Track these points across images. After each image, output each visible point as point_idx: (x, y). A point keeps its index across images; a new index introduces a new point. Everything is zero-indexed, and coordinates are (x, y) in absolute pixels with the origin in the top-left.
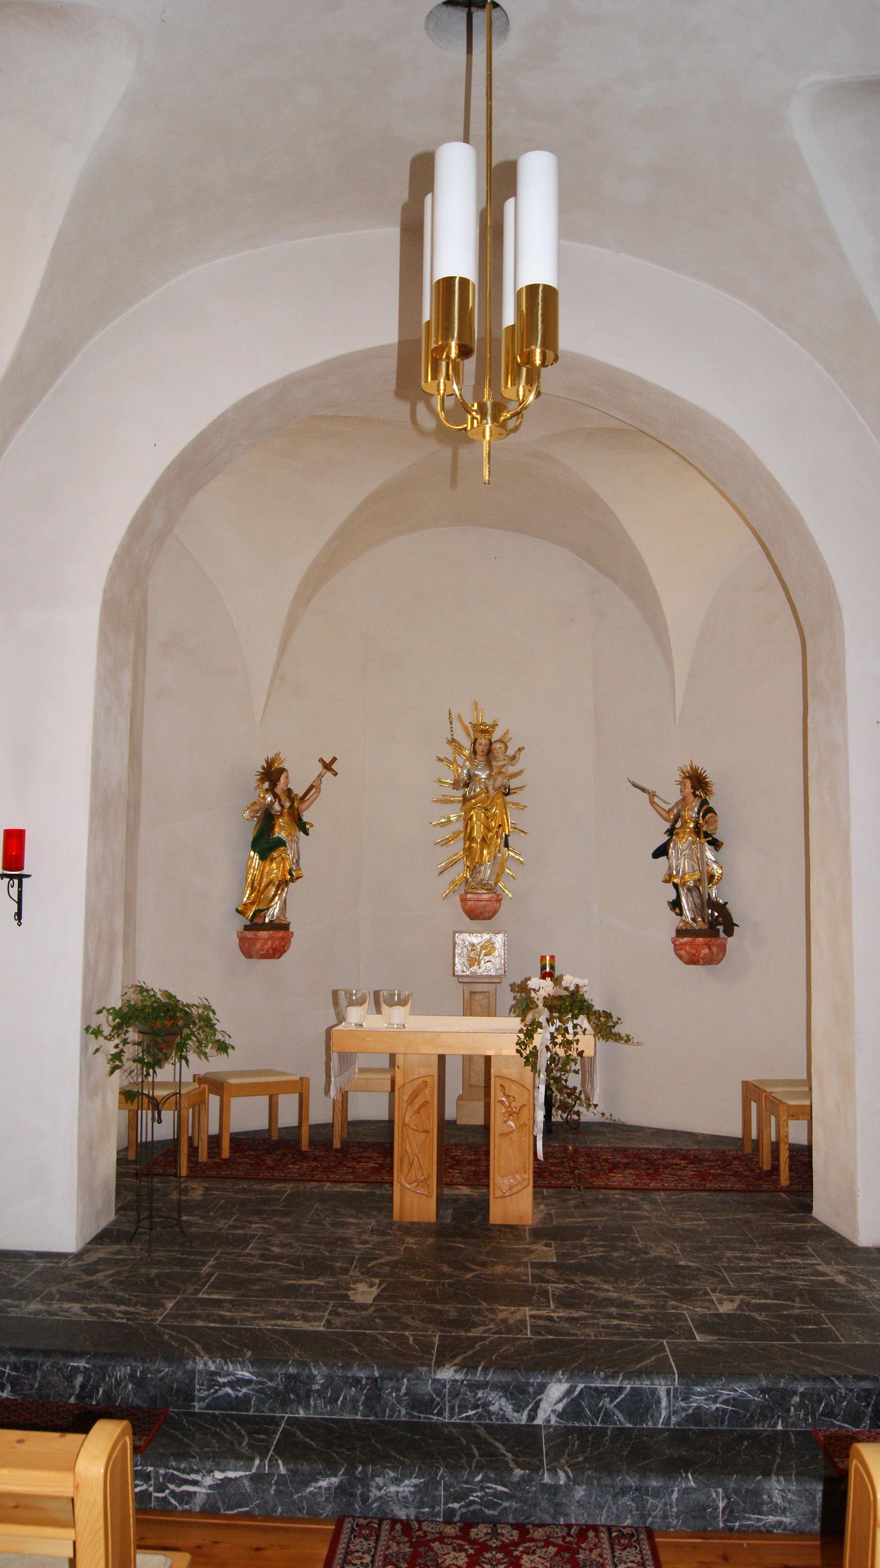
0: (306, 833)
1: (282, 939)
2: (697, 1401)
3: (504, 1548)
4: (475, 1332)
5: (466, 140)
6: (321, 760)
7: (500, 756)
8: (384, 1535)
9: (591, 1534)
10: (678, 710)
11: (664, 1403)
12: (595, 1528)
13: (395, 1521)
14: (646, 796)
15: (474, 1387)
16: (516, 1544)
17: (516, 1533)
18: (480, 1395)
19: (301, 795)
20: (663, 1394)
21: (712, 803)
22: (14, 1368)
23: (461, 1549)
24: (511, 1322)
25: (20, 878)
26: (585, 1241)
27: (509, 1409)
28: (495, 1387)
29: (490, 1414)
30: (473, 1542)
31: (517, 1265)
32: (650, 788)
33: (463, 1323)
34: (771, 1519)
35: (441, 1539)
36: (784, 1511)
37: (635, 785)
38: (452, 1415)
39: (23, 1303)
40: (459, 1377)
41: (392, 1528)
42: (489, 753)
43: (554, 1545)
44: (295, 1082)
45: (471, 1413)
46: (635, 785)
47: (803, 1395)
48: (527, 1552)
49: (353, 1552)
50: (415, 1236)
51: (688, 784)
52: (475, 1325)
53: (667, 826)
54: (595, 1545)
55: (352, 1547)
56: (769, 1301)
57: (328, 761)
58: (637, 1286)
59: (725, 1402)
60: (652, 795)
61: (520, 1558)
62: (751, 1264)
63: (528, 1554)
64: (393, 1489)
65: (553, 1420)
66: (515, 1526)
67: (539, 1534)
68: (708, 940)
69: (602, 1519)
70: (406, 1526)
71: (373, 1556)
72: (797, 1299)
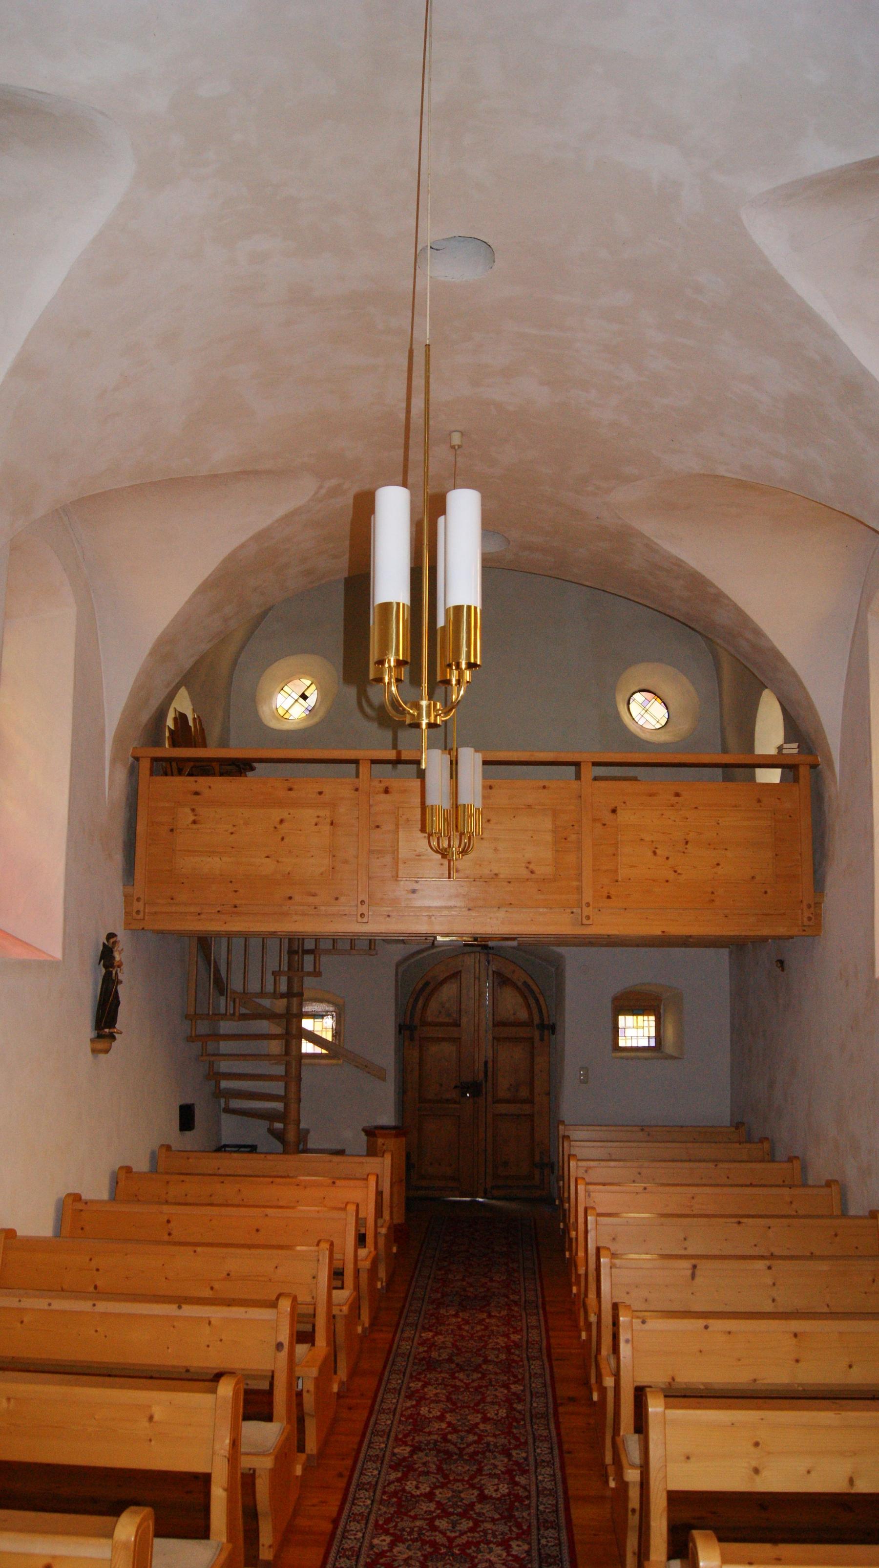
5: (405, 485)
23: (479, 1514)
35: (493, 1520)
43: (410, 1516)
48: (431, 1512)
49: (348, 1531)
54: (381, 1515)
55: (348, 1528)
61: (435, 1509)
63: (430, 1511)
71: (364, 1534)
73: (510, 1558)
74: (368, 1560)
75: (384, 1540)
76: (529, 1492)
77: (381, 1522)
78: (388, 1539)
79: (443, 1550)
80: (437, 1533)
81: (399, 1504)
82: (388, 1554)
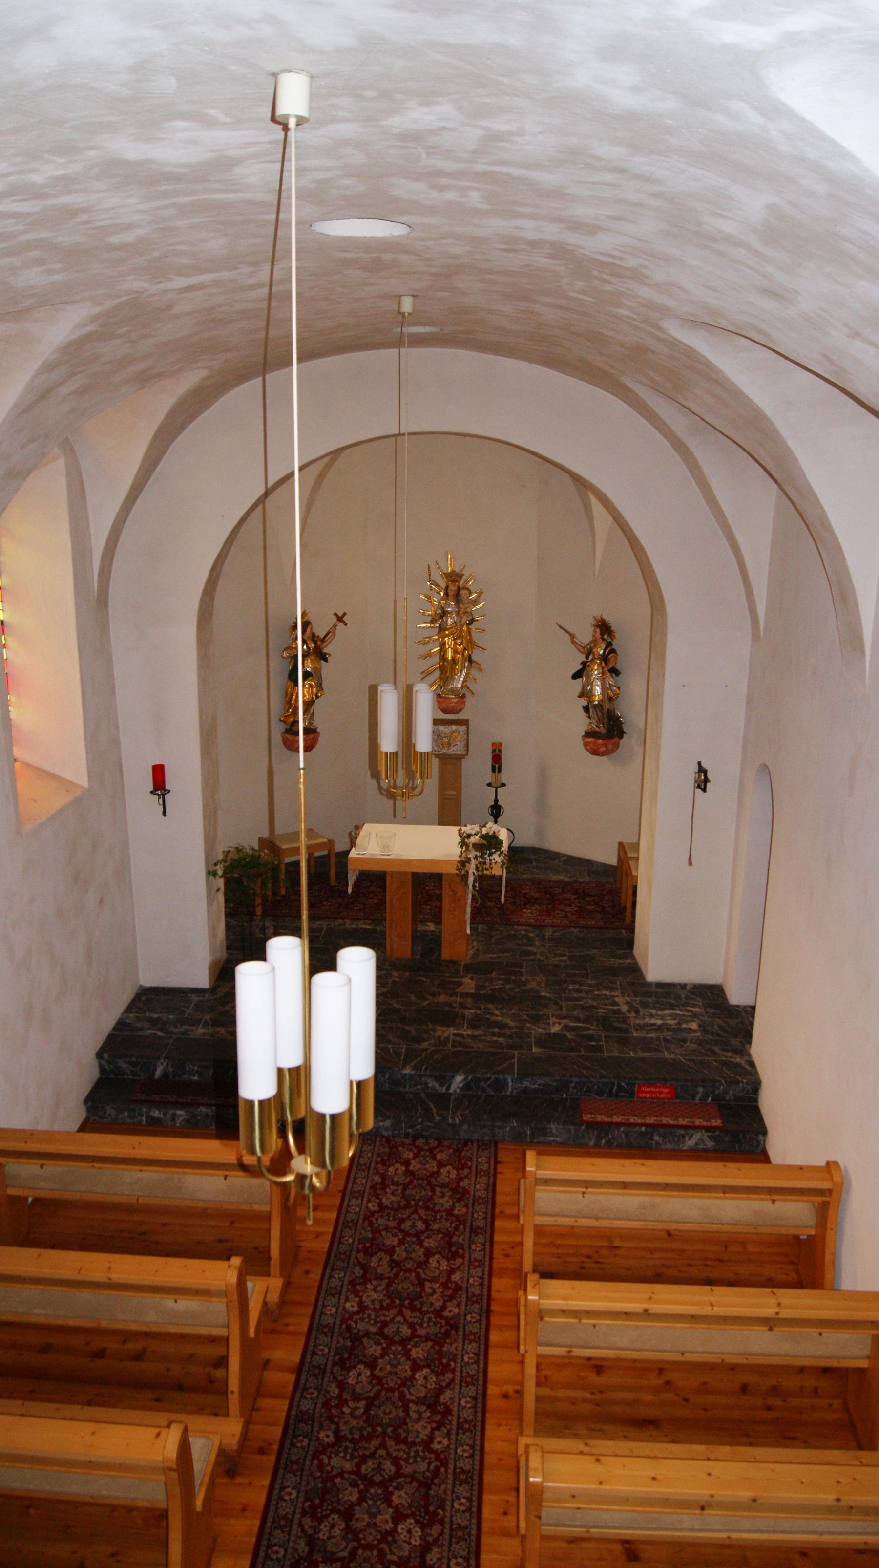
0: (326, 660)
1: (313, 739)
2: (526, 1084)
3: (430, 1150)
4: (424, 1045)
6: (336, 614)
7: (466, 601)
8: (377, 1143)
9: (470, 1143)
10: (597, 565)
11: (510, 1084)
12: (472, 1141)
13: (382, 1137)
14: (568, 637)
15: (420, 1076)
16: (435, 1148)
17: (436, 1143)
18: (423, 1079)
19: (322, 636)
20: (510, 1080)
21: (616, 645)
22: (199, 1066)
23: (411, 1150)
24: (443, 1038)
25: (164, 795)
26: (494, 975)
27: (437, 1086)
28: (430, 1076)
29: (428, 1088)
30: (416, 1147)
31: (452, 995)
32: (571, 632)
33: (419, 1039)
34: (551, 1139)
35: (403, 1145)
36: (557, 1136)
37: (561, 627)
38: (410, 1087)
39: (194, 1028)
40: (413, 1072)
41: (381, 1140)
42: (457, 597)
43: (442, 1233)
44: (325, 843)
45: (419, 1087)
46: (561, 627)
47: (576, 1083)
50: (398, 970)
51: (598, 630)
52: (425, 1040)
53: (583, 658)
56: (579, 1025)
57: (340, 615)
58: (513, 1011)
59: (540, 1085)
60: (572, 637)
62: (581, 995)
64: (381, 1124)
65: (458, 1091)
66: (435, 1139)
67: (446, 1143)
68: (605, 742)
69: (475, 1137)
70: (388, 1140)
72: (594, 1023)
73: (336, 1420)
74: (450, 1418)
75: (450, 1311)
76: (375, 1168)
77: (462, 1227)
78: (456, 1212)
79: (421, 1203)
80: (410, 1320)
81: (460, 1158)
82: (434, 1425)
